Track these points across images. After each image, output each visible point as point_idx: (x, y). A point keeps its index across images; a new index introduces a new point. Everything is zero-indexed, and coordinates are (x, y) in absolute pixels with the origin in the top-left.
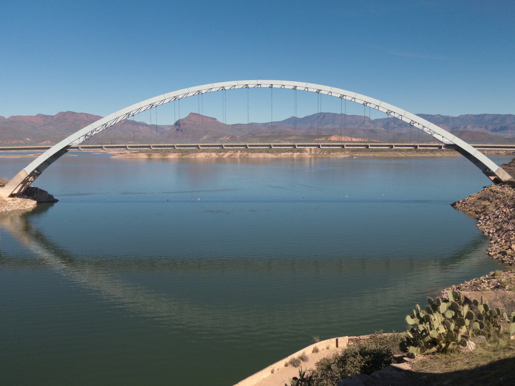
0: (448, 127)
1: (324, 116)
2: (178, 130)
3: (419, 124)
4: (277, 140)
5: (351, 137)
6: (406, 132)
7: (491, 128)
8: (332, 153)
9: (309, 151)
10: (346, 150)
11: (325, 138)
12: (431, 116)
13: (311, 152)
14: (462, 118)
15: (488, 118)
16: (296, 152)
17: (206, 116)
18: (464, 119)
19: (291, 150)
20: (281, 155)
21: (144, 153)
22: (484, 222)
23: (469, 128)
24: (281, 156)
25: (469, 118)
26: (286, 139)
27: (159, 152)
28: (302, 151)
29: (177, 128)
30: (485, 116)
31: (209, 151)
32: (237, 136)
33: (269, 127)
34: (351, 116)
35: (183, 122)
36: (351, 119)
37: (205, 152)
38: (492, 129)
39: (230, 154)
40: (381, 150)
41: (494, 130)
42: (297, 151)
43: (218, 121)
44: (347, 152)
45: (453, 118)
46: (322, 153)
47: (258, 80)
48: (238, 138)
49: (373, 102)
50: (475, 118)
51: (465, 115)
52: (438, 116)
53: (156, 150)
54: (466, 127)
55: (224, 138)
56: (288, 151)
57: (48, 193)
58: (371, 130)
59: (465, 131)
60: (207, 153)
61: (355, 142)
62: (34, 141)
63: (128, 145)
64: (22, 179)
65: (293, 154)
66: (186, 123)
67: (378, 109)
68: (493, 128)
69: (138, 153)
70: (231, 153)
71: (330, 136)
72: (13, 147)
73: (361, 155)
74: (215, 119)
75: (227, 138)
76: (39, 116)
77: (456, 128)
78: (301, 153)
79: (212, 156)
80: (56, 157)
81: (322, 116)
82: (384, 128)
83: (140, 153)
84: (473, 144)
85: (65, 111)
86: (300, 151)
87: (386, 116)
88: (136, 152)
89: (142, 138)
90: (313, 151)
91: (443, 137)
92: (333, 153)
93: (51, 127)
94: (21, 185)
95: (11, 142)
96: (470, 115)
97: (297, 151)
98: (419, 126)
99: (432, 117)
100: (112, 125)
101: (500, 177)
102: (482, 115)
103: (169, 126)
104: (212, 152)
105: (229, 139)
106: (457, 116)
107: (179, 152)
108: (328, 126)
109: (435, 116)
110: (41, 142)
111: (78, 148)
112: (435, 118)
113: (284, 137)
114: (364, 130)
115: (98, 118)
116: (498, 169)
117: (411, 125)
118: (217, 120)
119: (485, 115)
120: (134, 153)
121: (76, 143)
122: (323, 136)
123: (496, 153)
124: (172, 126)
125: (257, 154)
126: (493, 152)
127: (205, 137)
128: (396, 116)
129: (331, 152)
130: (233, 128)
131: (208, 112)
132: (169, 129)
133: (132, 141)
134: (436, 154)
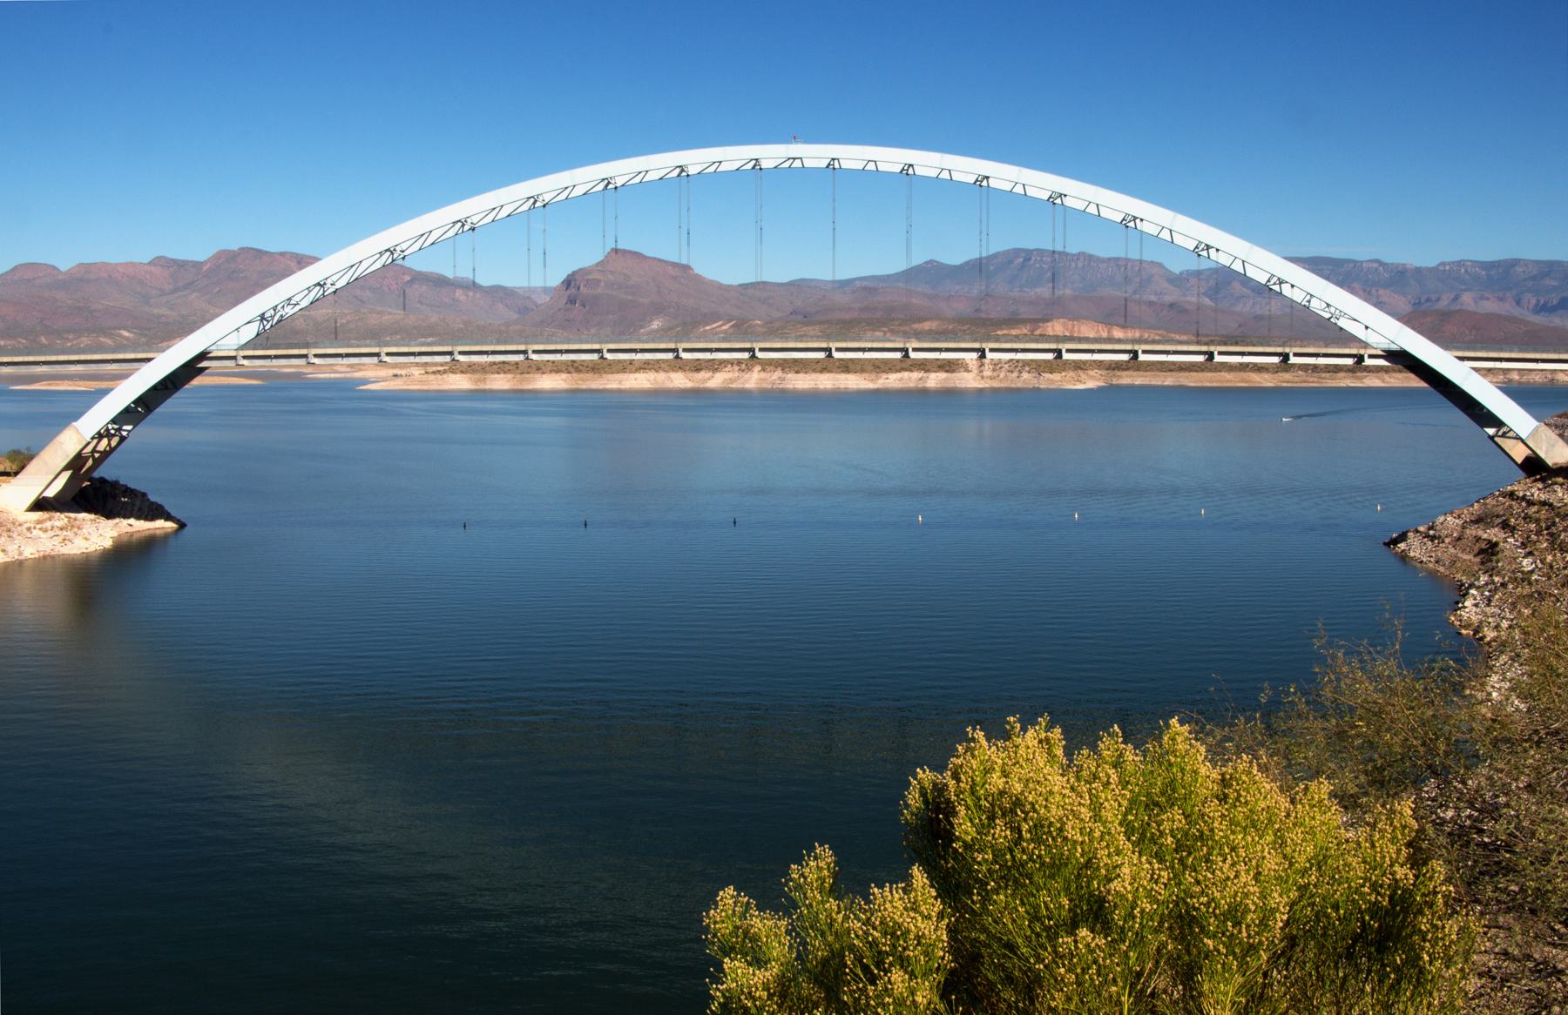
0: (1405, 297)
1: (1027, 259)
2: (572, 301)
3: (1293, 286)
4: (881, 334)
5: (1110, 324)
6: (1279, 313)
7: (1533, 302)
8: (1048, 376)
9: (974, 368)
10: (1090, 365)
11: (1028, 327)
12: (1351, 265)
13: (981, 372)
14: (1445, 270)
15: (1524, 272)
16: (935, 369)
17: (659, 260)
18: (1451, 275)
19: (920, 365)
20: (887, 379)
21: (462, 372)
22: (1487, 593)
23: (1468, 301)
24: (887, 381)
25: (1466, 271)
26: (907, 328)
27: (509, 370)
28: (954, 367)
29: (569, 296)
30: (1515, 265)
31: (663, 365)
32: (753, 320)
33: (854, 292)
34: (1109, 259)
35: (590, 277)
36: (1110, 269)
37: (650, 369)
38: (1537, 305)
39: (730, 375)
40: (1199, 367)
41: (1542, 309)
42: (939, 367)
43: (697, 274)
44: (1091, 373)
45: (1418, 270)
46: (1015, 374)
47: (791, 143)
48: (757, 325)
49: (1155, 218)
50: (1484, 273)
51: (1453, 262)
52: (1375, 265)
53: (500, 363)
54: (1456, 298)
55: (714, 325)
56: (911, 365)
57: (148, 500)
58: (1171, 305)
59: (1457, 311)
60: (657, 371)
61: (1119, 341)
62: (143, 339)
63: (532, 347)
64: (68, 456)
65: (925, 375)
66: (599, 281)
67: (1170, 240)
68: (1538, 301)
69: (445, 372)
70: (731, 373)
71: (1046, 320)
72: (83, 357)
73: (1138, 382)
74: (686, 268)
75: (724, 328)
76: (160, 261)
77: (1428, 300)
78: (949, 375)
79: (672, 382)
80: (170, 386)
81: (1021, 260)
82: (1211, 300)
83: (453, 372)
84: (1458, 349)
85: (234, 246)
86: (948, 368)
87: (1193, 265)
88: (439, 371)
89: (462, 326)
90: (987, 368)
91: (1367, 328)
92: (1051, 373)
93: (194, 295)
94: (64, 473)
95: (75, 342)
96: (1471, 261)
97: (939, 367)
98: (1292, 293)
99: (1355, 266)
100: (339, 285)
101: (1542, 455)
102: (1506, 261)
103: (545, 290)
104: (673, 371)
105: (731, 331)
106: (1432, 264)
107: (571, 369)
108: (1039, 290)
109: (1364, 264)
110: (162, 342)
111: (234, 358)
112: (1365, 270)
113: (900, 325)
114: (1151, 303)
115: (303, 261)
116: (1536, 429)
117: (1264, 290)
118: (692, 269)
119: (1514, 263)
120: (434, 373)
121: (229, 345)
122: (1023, 322)
123: (1546, 377)
124: (555, 289)
125: (814, 376)
126: (1536, 375)
127: (656, 325)
128: (1224, 260)
129: (1043, 372)
130: (741, 295)
131: (660, 244)
132: (543, 299)
133: (433, 337)
134: (1364, 380)
